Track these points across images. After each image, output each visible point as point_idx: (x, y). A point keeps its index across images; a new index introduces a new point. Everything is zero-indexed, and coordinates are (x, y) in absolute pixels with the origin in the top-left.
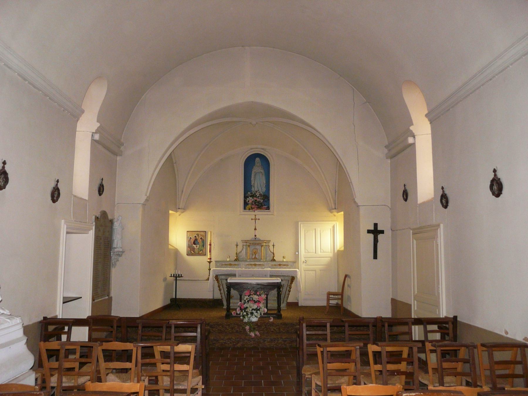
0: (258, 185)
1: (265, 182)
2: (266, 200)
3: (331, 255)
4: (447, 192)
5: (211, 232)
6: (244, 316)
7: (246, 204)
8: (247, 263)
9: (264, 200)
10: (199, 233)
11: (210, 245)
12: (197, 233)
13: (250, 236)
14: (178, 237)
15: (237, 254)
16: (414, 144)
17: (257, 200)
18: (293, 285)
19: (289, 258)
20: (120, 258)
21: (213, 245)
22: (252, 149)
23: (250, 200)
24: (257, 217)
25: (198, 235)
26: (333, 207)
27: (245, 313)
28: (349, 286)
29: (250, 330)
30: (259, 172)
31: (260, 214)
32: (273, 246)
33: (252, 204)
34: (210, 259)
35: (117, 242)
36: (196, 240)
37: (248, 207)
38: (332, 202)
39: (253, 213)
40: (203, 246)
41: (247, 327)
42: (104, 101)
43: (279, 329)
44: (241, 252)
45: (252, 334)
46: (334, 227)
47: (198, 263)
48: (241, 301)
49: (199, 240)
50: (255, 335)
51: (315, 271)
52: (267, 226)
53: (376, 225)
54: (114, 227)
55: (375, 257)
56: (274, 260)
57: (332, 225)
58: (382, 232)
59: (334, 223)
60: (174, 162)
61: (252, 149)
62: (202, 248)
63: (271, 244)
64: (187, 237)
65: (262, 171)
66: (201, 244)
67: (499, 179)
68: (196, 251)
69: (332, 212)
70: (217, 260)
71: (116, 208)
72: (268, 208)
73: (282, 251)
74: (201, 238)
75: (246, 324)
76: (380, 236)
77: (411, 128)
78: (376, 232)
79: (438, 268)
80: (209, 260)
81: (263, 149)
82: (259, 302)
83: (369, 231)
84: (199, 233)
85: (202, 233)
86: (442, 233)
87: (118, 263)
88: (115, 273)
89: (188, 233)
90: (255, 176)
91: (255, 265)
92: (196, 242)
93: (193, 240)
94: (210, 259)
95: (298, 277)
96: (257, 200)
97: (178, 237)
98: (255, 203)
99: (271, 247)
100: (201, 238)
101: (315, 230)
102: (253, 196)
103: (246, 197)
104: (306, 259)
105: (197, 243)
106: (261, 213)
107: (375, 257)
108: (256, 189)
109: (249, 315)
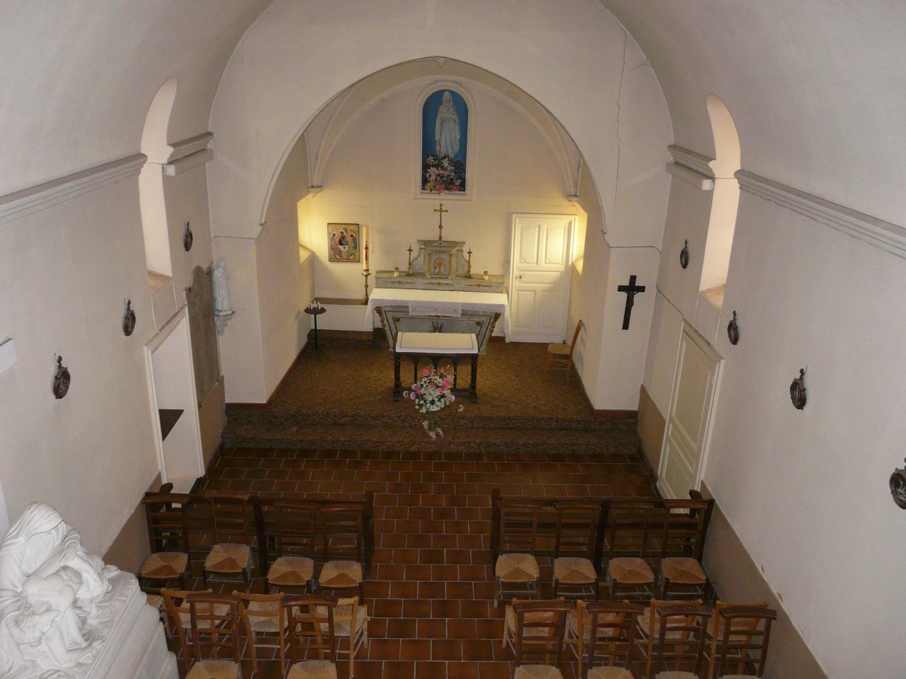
0: (446, 142)
1: (458, 136)
3: (562, 268)
4: (739, 323)
5: (367, 227)
6: (421, 406)
7: (425, 181)
8: (427, 281)
10: (349, 228)
11: (367, 248)
12: (344, 226)
13: (433, 235)
14: (314, 233)
15: (410, 264)
16: (711, 193)
17: (445, 172)
18: (497, 323)
19: (495, 269)
20: (229, 322)
21: (370, 246)
22: (437, 81)
25: (346, 230)
27: (422, 402)
28: (582, 339)
29: (430, 429)
31: (447, 199)
32: (470, 253)
34: (367, 270)
35: (222, 303)
36: (343, 237)
37: (429, 185)
38: (572, 184)
39: (436, 196)
40: (355, 248)
41: (425, 424)
42: (175, 101)
43: (472, 423)
44: (416, 259)
45: (433, 435)
46: (570, 224)
47: (349, 275)
48: (416, 383)
49: (349, 239)
50: (437, 434)
51: (535, 291)
52: (461, 218)
53: (633, 278)
54: (214, 280)
55: (626, 326)
56: (468, 276)
57: (568, 221)
58: (642, 289)
59: (572, 218)
62: (354, 251)
63: (466, 249)
64: (329, 234)
66: (352, 244)
67: (804, 390)
68: (345, 256)
69: (570, 201)
70: (380, 269)
71: (213, 245)
72: (462, 187)
73: (483, 262)
74: (352, 236)
75: (423, 416)
76: (638, 297)
77: (711, 164)
78: (632, 289)
79: (711, 385)
80: (365, 273)
81: (456, 82)
82: (443, 387)
83: (621, 288)
84: (349, 228)
85: (353, 228)
86: (721, 372)
87: (226, 329)
88: (224, 343)
89: (330, 227)
90: (442, 123)
91: (439, 284)
92: (343, 242)
93: (341, 239)
94: (367, 270)
95: (506, 315)
96: (445, 172)
97: (314, 233)
99: (466, 256)
100: (352, 236)
101: (539, 227)
103: (425, 167)
104: (521, 273)
105: (345, 243)
106: (449, 197)
107: (626, 326)
109: (429, 405)
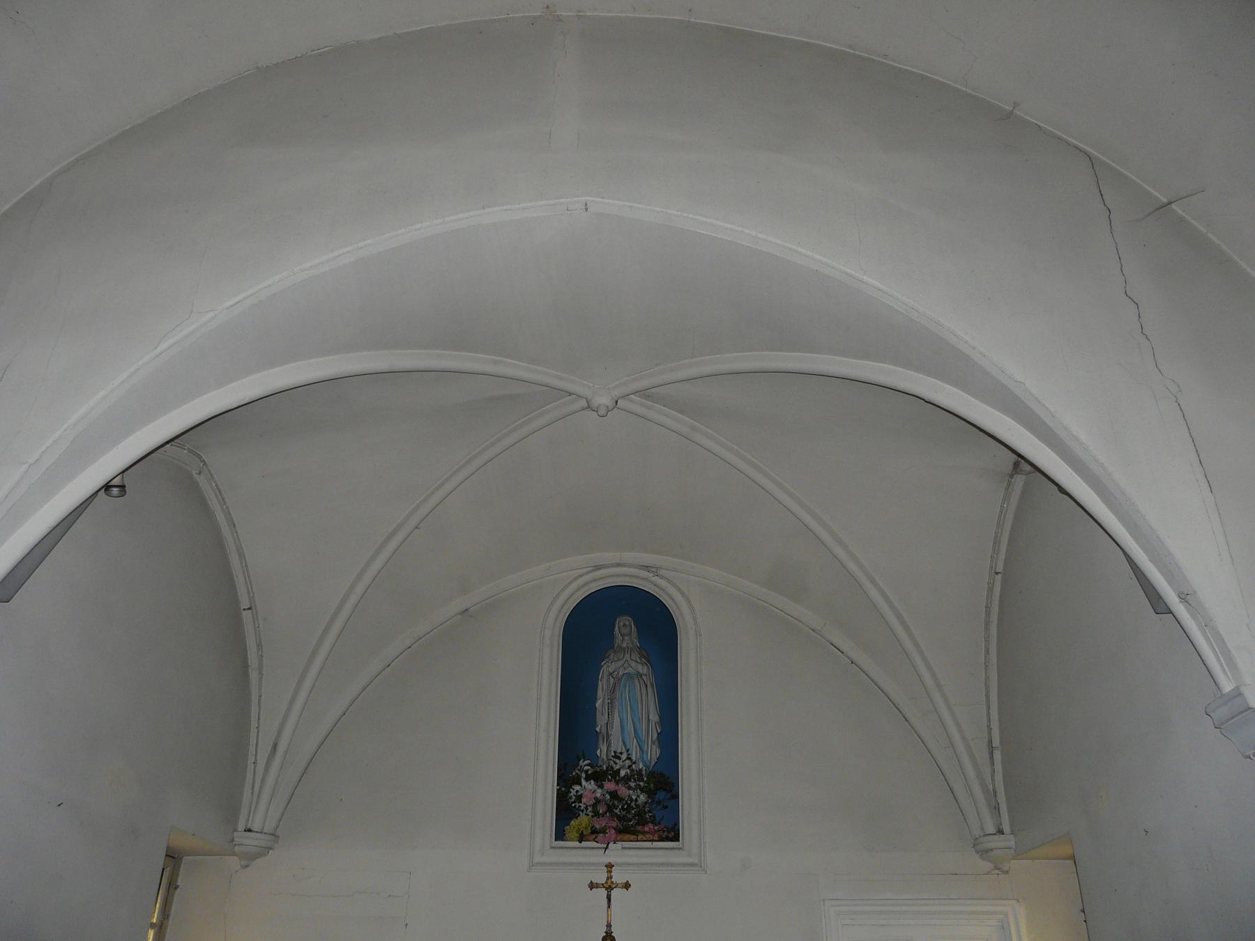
0: (624, 731)
1: (654, 717)
2: (661, 795)
7: (565, 810)
9: (651, 793)
22: (598, 568)
23: (588, 789)
24: (618, 877)
26: (991, 828)
30: (629, 676)
31: (627, 856)
33: (596, 814)
60: (245, 603)
61: (598, 568)
65: (643, 669)
72: (672, 833)
81: (646, 568)
98: (610, 809)
102: (598, 777)
103: (566, 778)
108: (617, 746)
